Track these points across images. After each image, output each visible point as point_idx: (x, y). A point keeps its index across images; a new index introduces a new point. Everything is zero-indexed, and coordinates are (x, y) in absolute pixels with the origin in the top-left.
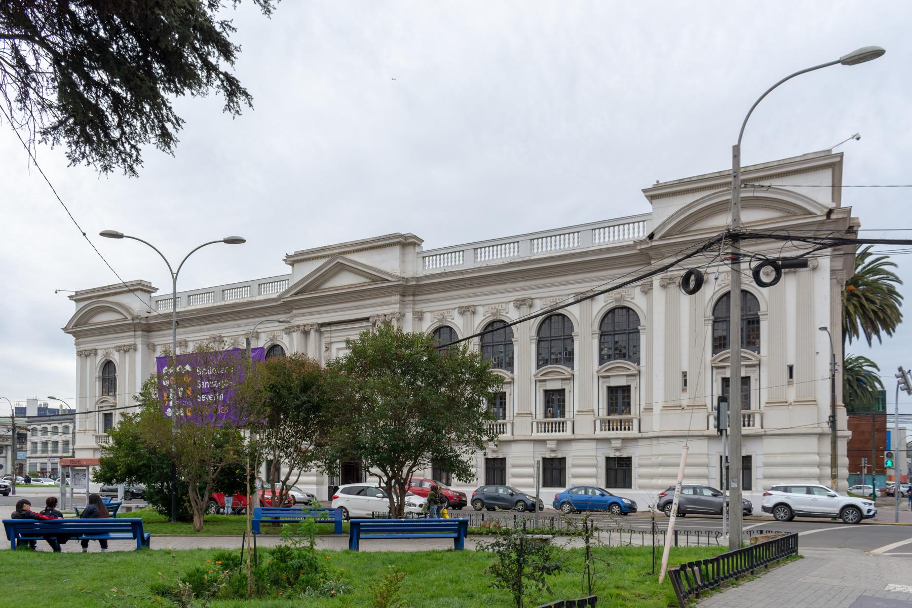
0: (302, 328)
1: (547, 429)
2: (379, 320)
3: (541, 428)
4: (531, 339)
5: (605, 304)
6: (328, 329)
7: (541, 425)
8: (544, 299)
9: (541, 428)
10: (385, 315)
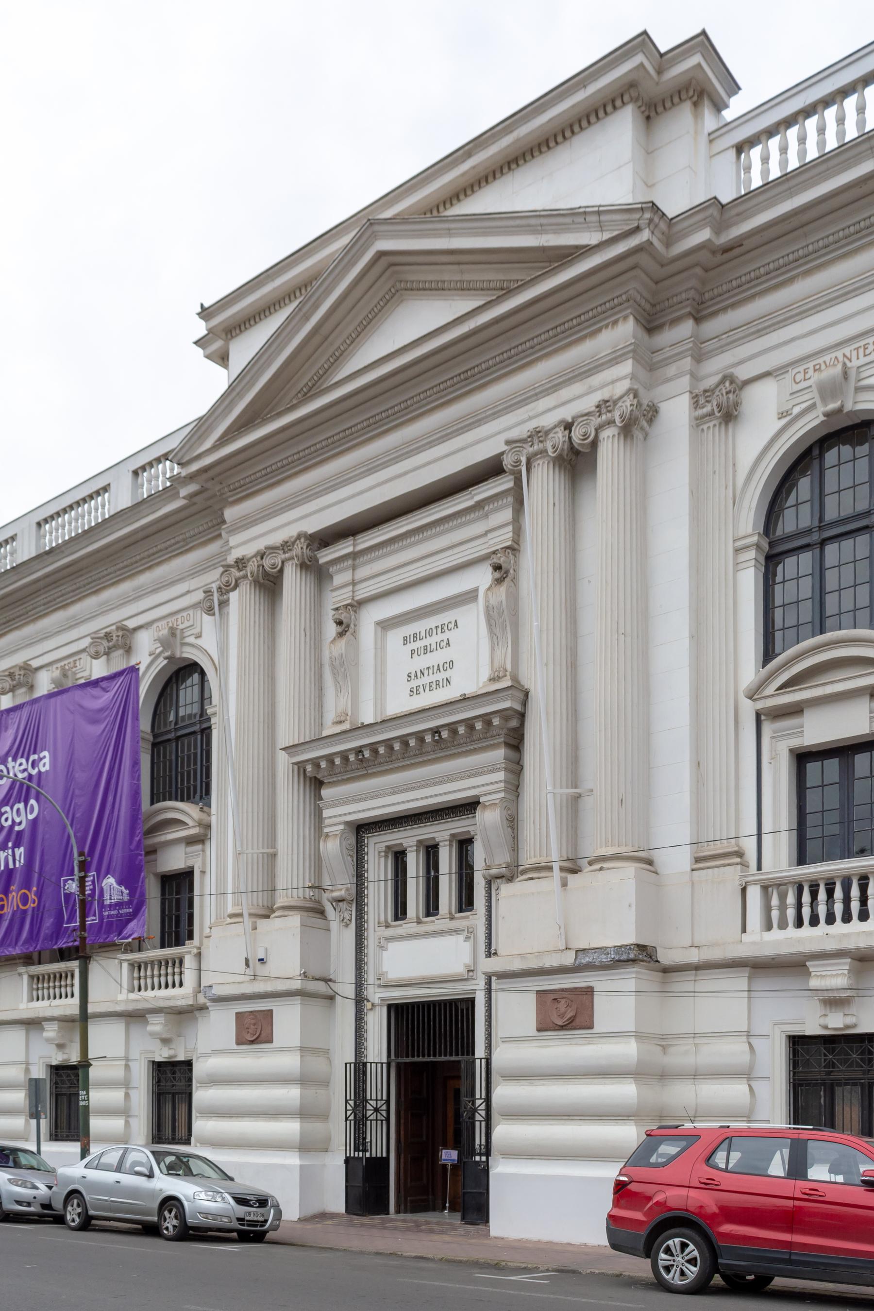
0: (252, 566)
1: (806, 911)
2: (544, 452)
3: (783, 907)
4: (737, 551)
5: (784, 421)
6: (345, 548)
7: (783, 897)
8: (792, 372)
9: (783, 907)
10: (568, 426)
